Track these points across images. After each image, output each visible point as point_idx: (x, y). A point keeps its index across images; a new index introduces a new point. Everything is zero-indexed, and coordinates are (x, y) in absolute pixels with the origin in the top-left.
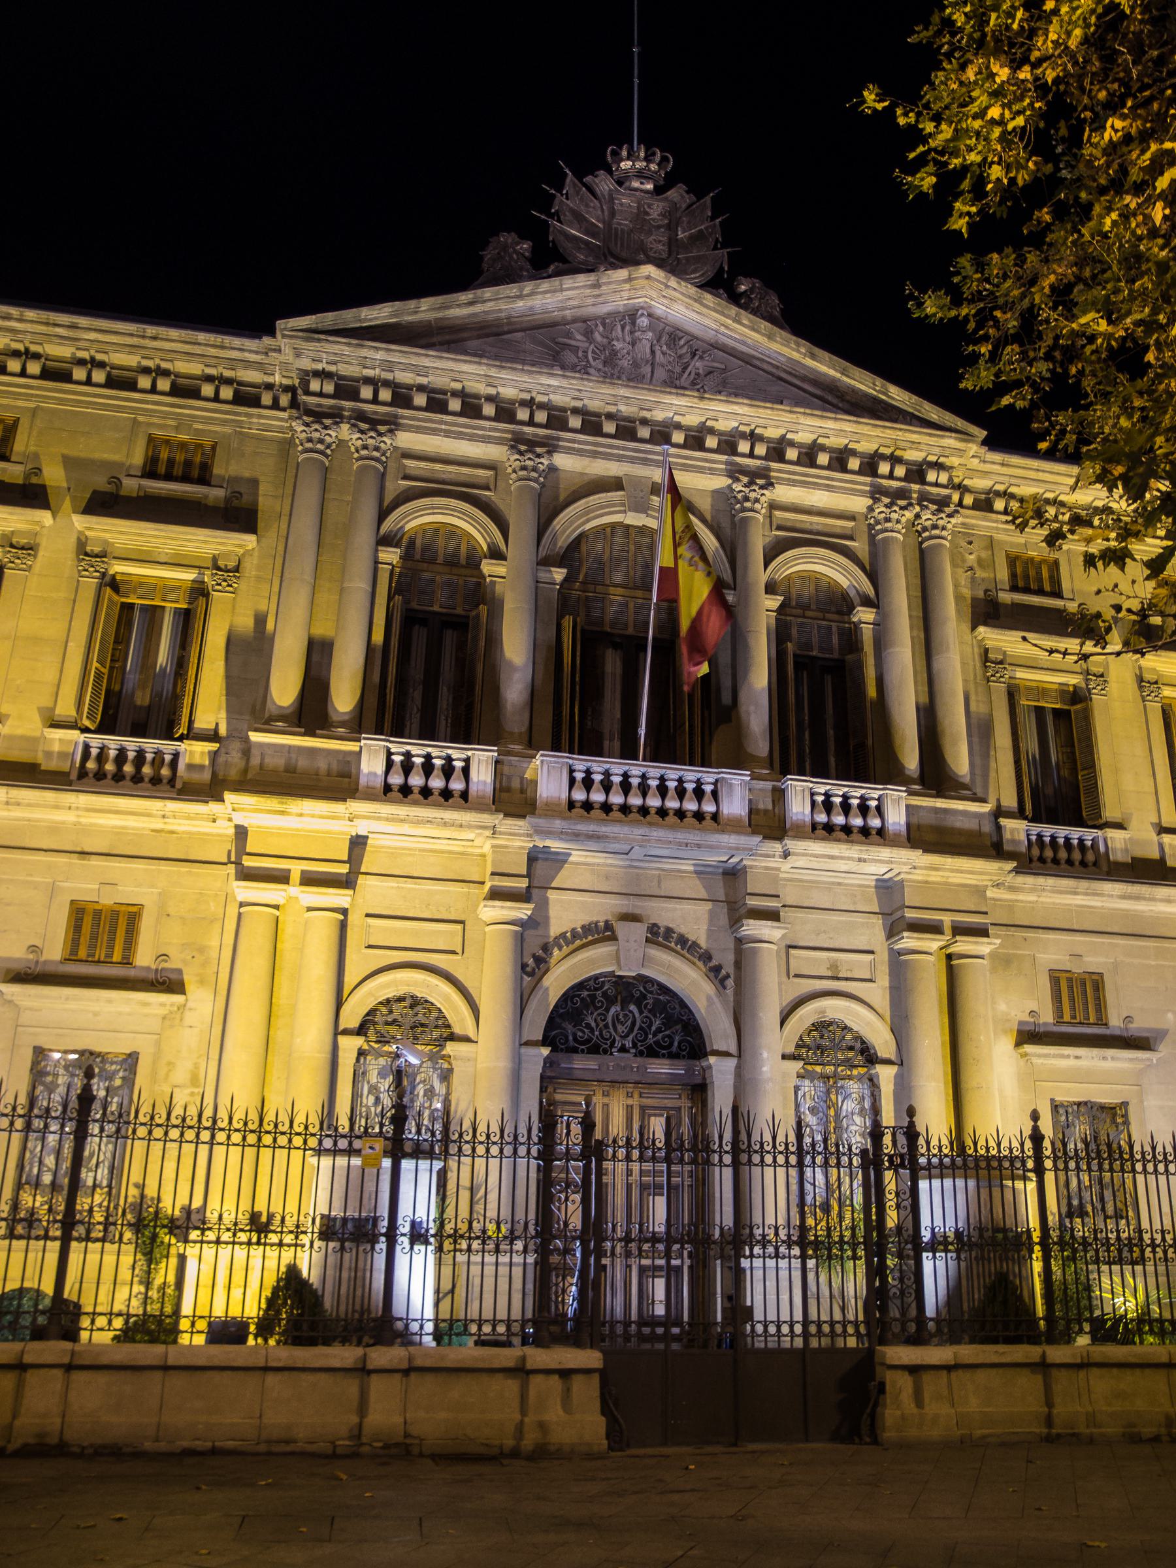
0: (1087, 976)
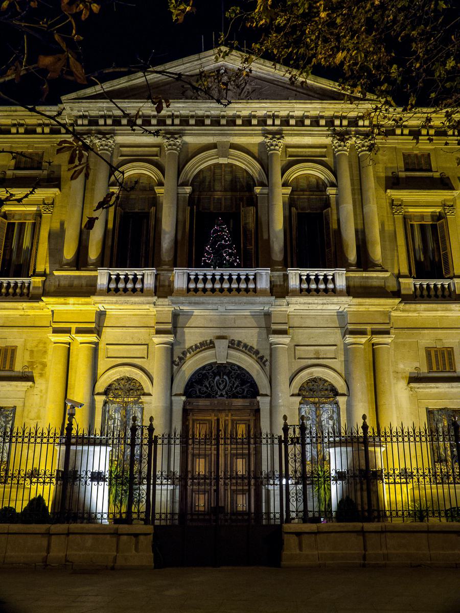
0: (445, 349)
